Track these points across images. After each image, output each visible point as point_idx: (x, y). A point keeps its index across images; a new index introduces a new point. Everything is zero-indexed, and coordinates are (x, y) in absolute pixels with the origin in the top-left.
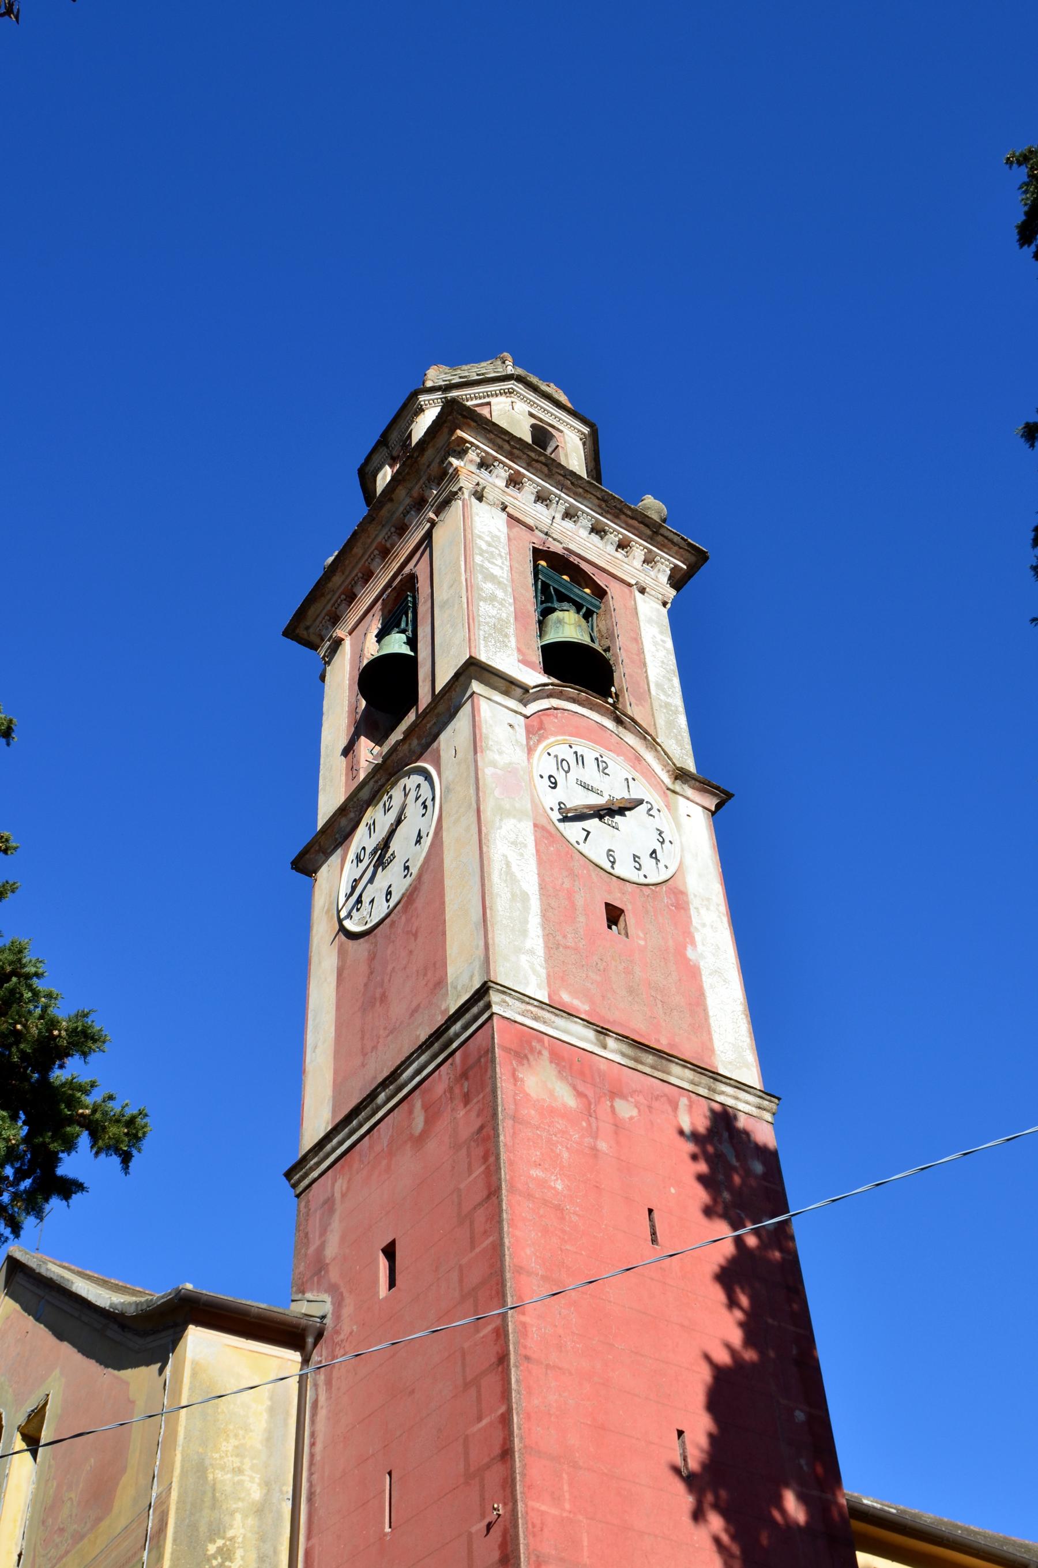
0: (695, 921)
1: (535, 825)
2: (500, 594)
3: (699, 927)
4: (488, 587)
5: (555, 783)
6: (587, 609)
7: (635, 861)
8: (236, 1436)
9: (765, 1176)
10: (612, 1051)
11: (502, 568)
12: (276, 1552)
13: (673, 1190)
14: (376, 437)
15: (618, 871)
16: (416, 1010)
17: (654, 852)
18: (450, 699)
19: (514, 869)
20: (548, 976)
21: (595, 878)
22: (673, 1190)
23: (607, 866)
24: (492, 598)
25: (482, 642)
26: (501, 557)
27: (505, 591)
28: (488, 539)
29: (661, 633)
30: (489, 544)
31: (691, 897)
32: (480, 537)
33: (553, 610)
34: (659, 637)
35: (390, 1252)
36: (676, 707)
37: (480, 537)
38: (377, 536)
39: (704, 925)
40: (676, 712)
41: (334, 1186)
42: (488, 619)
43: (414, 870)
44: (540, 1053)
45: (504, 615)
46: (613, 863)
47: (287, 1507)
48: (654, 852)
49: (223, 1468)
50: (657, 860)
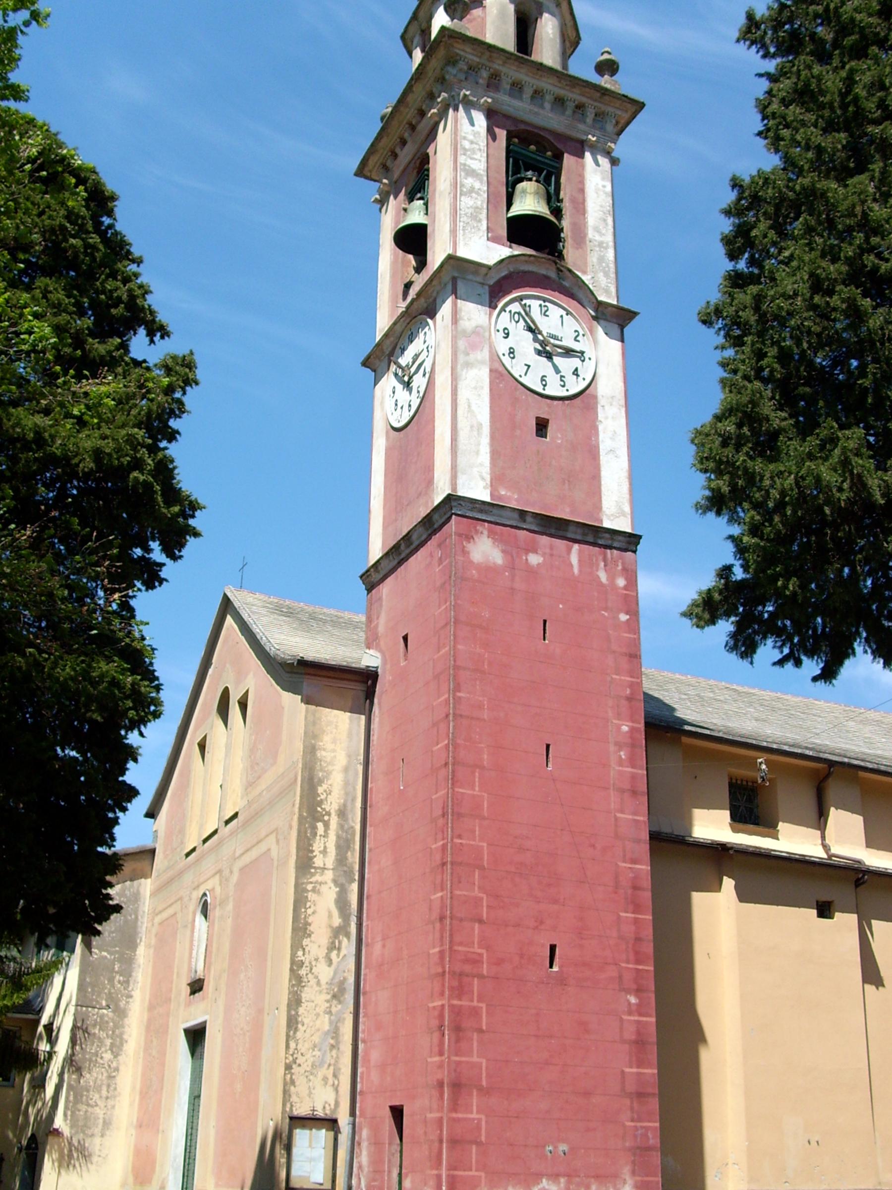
0: (601, 415)
1: (491, 371)
2: (477, 185)
3: (602, 420)
4: (469, 181)
5: (508, 334)
6: (548, 171)
7: (562, 380)
8: (331, 733)
9: (626, 588)
10: (530, 523)
11: (480, 161)
12: (355, 789)
13: (561, 606)
14: (410, 14)
15: (548, 392)
16: (420, 494)
17: (576, 369)
18: (440, 277)
19: (474, 407)
20: (491, 479)
21: (530, 399)
22: (561, 606)
23: (539, 389)
24: (472, 190)
25: (461, 232)
26: (480, 150)
27: (481, 183)
28: (471, 137)
29: (603, 179)
30: (472, 142)
31: (600, 397)
32: (465, 138)
33: (521, 180)
34: (601, 183)
35: (405, 638)
36: (607, 243)
37: (465, 138)
38: (407, 114)
39: (607, 418)
40: (606, 248)
41: (386, 589)
42: (467, 210)
43: (605, 81)
44: (482, 533)
45: (479, 203)
46: (545, 386)
47: (360, 768)
48: (576, 369)
49: (324, 750)
50: (578, 375)
